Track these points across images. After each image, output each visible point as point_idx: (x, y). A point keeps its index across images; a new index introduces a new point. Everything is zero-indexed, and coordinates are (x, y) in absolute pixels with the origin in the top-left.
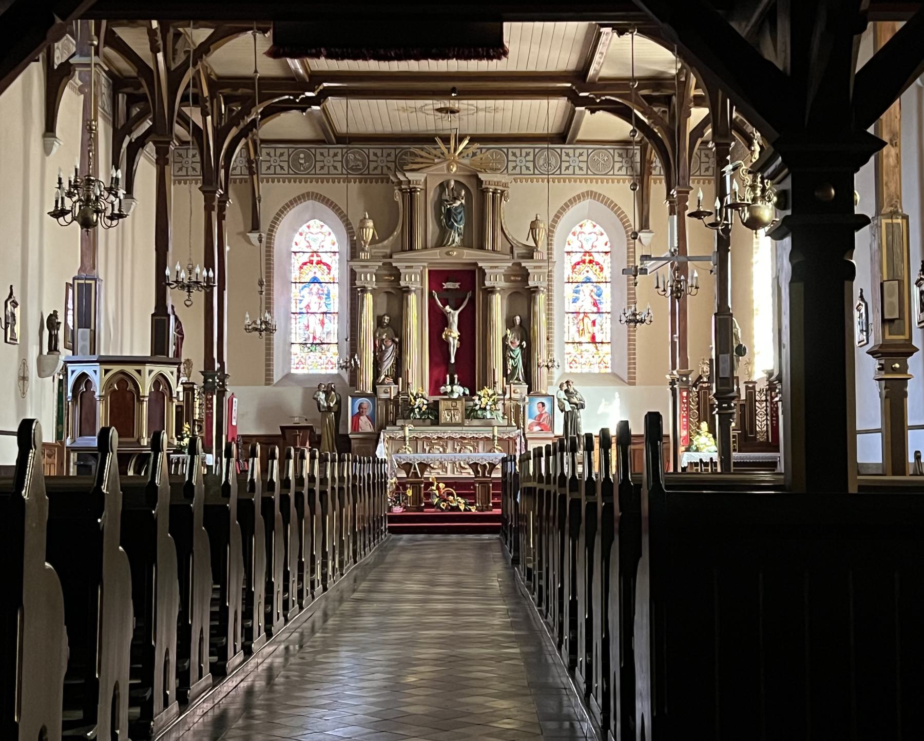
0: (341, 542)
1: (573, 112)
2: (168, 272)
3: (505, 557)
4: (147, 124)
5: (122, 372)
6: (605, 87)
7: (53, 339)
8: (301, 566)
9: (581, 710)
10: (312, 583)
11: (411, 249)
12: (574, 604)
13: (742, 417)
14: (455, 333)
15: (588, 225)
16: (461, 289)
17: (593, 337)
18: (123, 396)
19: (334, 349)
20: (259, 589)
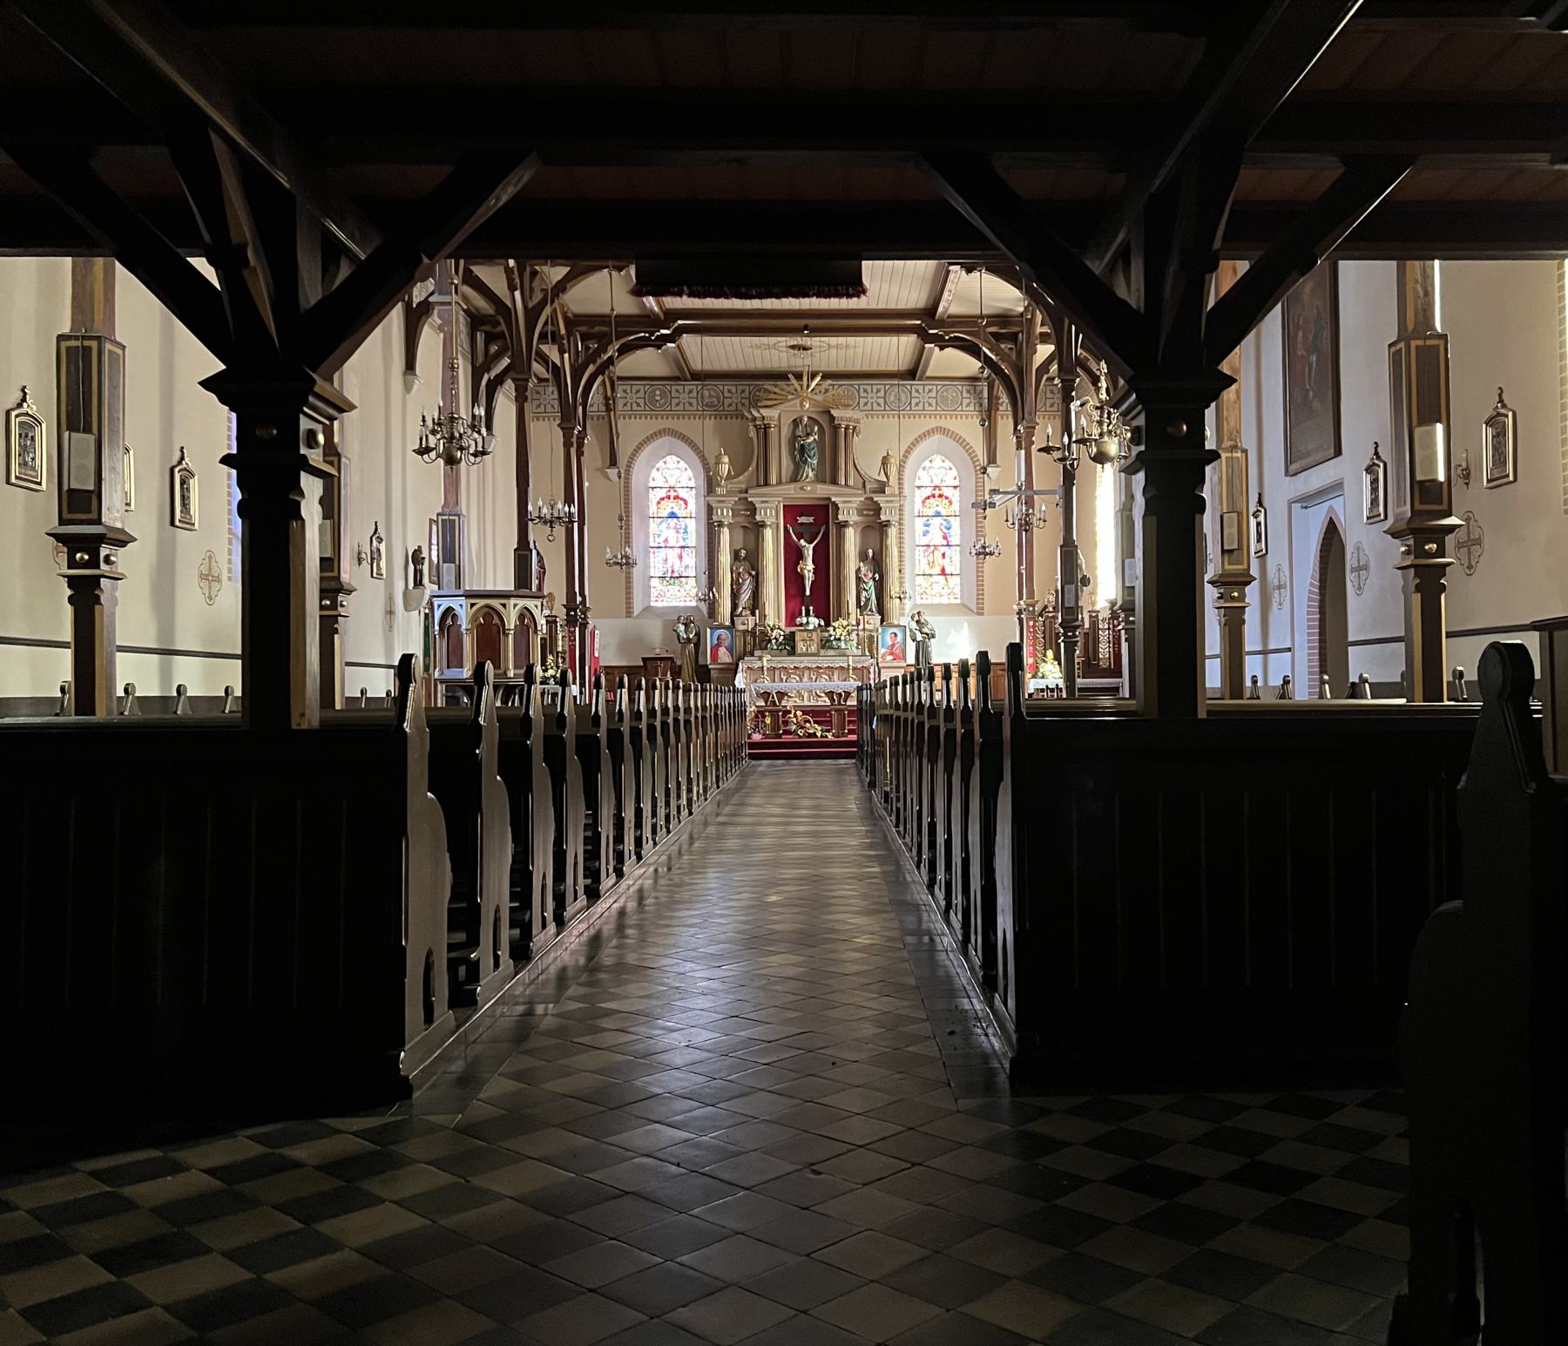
0: (705, 768)
2: (530, 508)
3: (861, 781)
4: (506, 361)
5: (488, 606)
6: (953, 325)
7: (418, 575)
8: (667, 791)
9: (941, 925)
10: (679, 808)
11: (766, 484)
12: (932, 825)
13: (1086, 644)
14: (810, 566)
15: (937, 459)
16: (815, 523)
17: (943, 570)
18: (489, 633)
19: (692, 582)
20: (629, 815)
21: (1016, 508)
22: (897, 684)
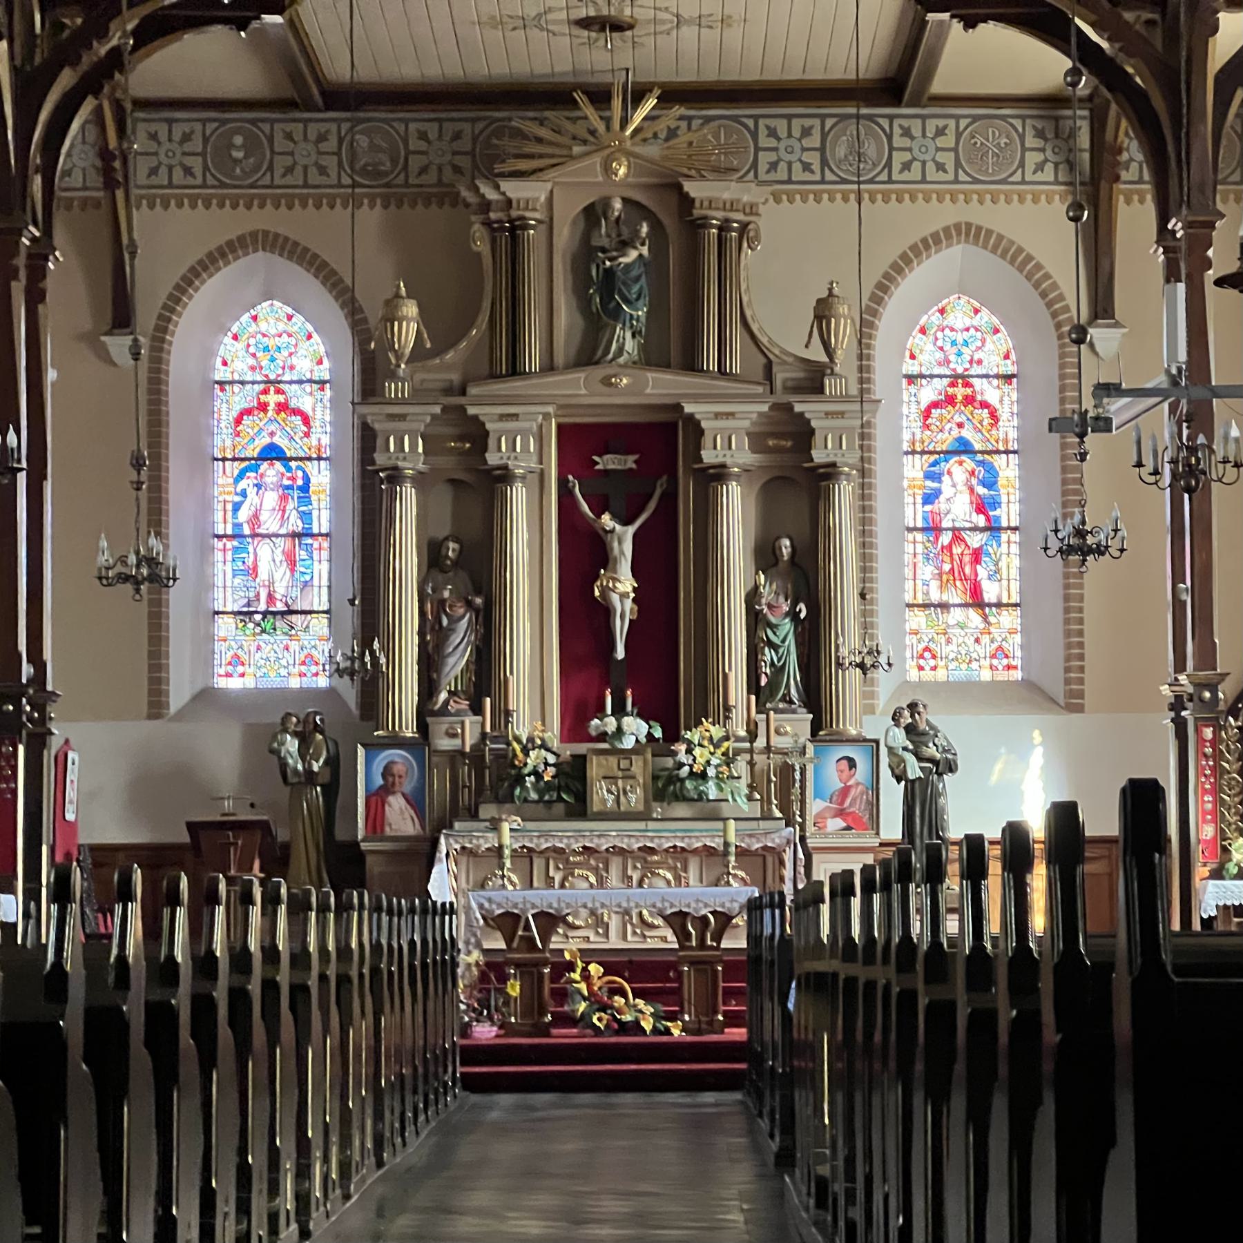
0: (345, 1117)
1: (920, 26)
3: (757, 1149)
8: (244, 1175)
10: (273, 1218)
11: (515, 370)
14: (626, 583)
16: (639, 472)
19: (320, 625)
21: (1161, 427)
22: (849, 891)
